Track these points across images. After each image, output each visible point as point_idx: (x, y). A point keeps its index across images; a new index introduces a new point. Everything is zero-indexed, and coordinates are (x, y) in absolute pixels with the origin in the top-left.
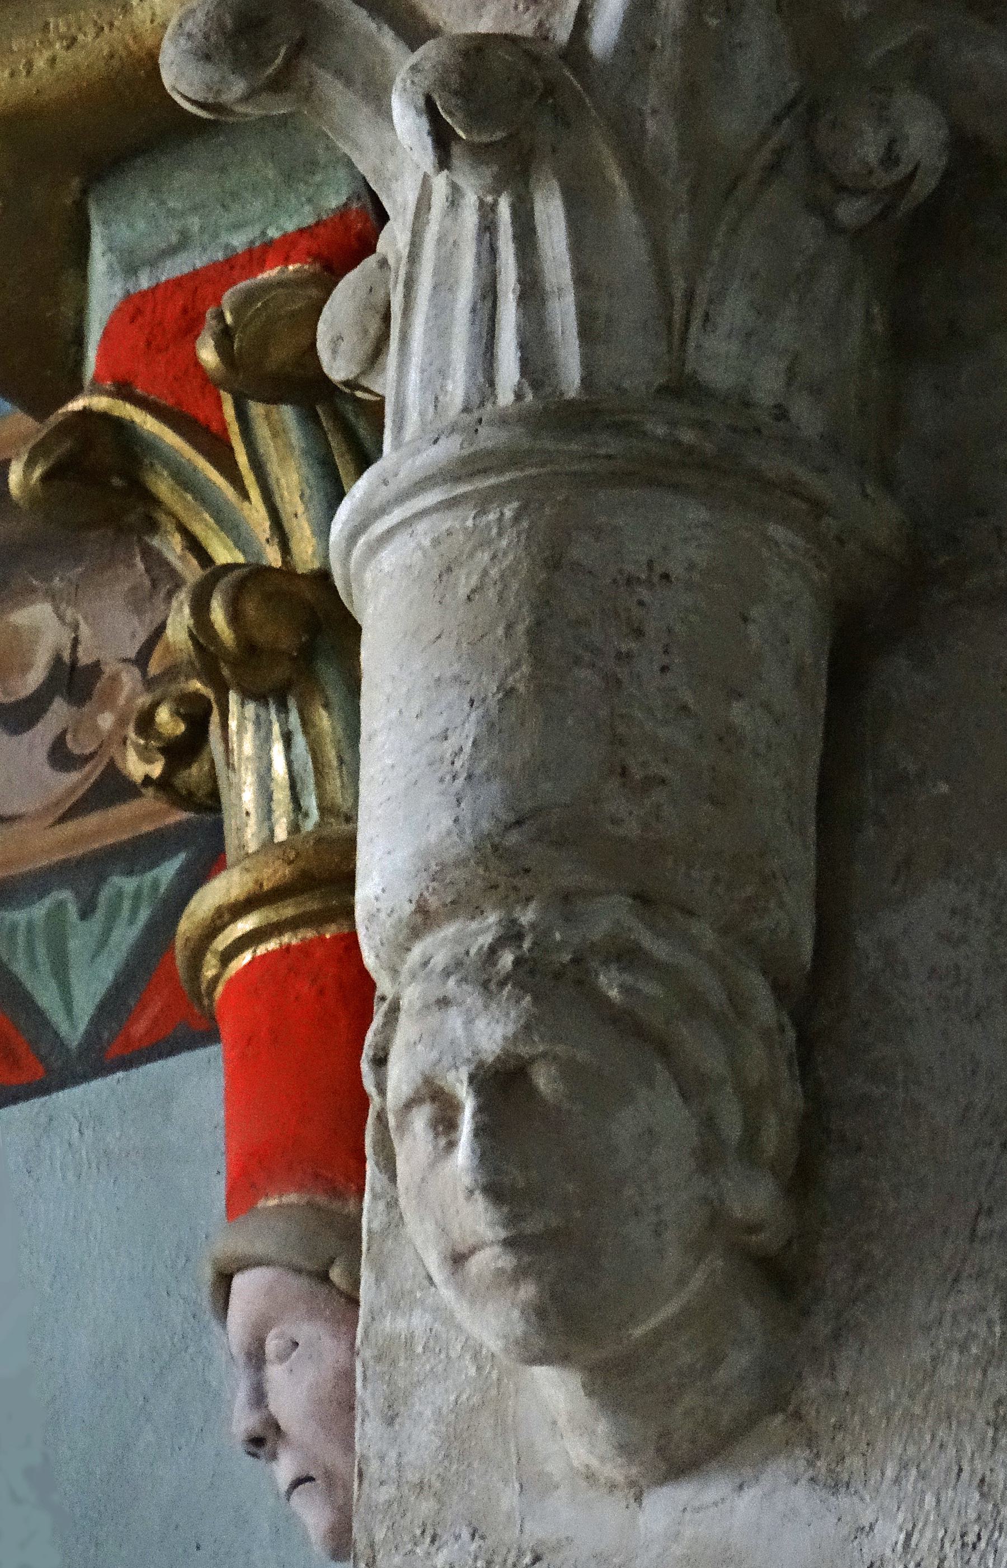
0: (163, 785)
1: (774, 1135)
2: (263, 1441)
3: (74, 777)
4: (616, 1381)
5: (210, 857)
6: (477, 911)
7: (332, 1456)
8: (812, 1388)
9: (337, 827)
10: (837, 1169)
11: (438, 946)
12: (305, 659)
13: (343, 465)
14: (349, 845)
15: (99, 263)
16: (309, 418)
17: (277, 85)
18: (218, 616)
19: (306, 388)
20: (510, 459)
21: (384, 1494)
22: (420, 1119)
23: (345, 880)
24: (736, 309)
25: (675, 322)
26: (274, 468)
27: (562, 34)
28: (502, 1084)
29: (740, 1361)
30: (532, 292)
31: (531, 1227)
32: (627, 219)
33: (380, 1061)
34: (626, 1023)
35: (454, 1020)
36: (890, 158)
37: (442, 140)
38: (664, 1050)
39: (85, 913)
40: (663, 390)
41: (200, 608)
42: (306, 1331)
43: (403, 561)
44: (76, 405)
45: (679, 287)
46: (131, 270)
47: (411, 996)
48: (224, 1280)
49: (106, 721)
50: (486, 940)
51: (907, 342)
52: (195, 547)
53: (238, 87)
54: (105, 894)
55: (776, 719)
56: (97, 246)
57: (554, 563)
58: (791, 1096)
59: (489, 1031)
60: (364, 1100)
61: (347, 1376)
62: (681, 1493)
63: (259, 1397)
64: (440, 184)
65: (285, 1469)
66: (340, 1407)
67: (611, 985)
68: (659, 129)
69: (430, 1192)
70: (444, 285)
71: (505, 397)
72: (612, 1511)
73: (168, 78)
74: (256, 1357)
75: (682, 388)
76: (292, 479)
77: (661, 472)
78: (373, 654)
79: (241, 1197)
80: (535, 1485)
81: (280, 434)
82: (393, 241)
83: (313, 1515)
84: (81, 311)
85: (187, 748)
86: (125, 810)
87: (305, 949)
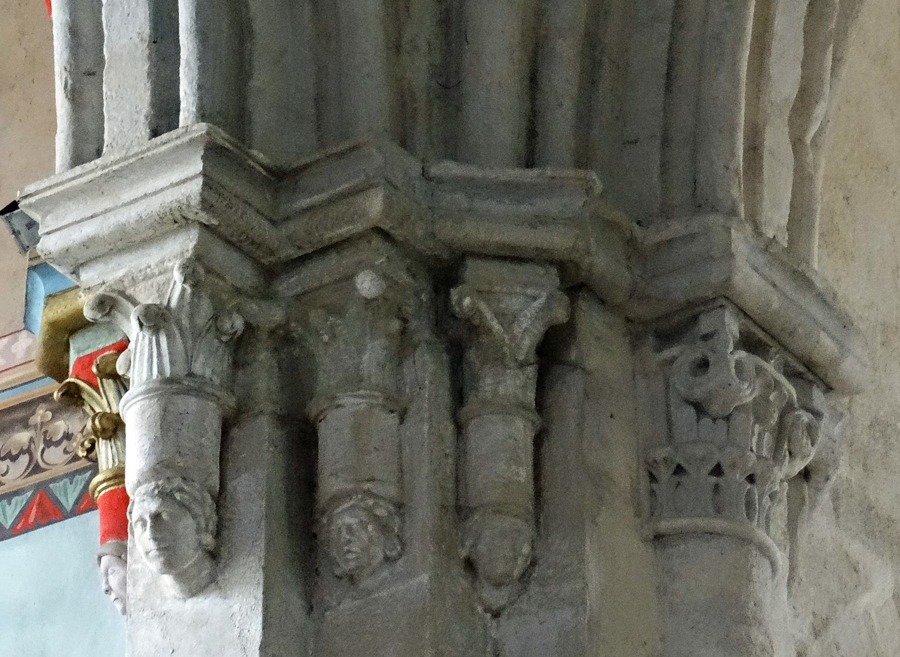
0: (86, 457)
1: (212, 527)
2: (108, 591)
3: (68, 456)
4: (181, 577)
5: (96, 472)
6: (150, 482)
7: (122, 593)
8: (220, 578)
9: (122, 466)
10: (225, 533)
11: (142, 489)
12: (115, 431)
13: (122, 390)
14: (123, 469)
15: (72, 352)
16: (115, 381)
17: (108, 314)
18: (97, 422)
19: (115, 377)
20: (156, 390)
21: (133, 602)
22: (139, 524)
23: (123, 476)
24: (201, 359)
25: (189, 360)
26: (108, 393)
27: (165, 303)
28: (156, 517)
29: (205, 573)
30: (160, 355)
31: (162, 546)
32: (179, 341)
33: (131, 513)
34: (182, 505)
35: (146, 504)
36: (232, 327)
37: (141, 325)
38: (189, 510)
39: (71, 483)
40: (187, 375)
41: (93, 420)
42: (117, 568)
43: (136, 411)
44: (67, 380)
45: (190, 354)
46: (78, 352)
47: (137, 500)
48: (100, 558)
49: (75, 444)
50: (152, 488)
51: (237, 365)
52: (92, 409)
53: (100, 315)
54: (75, 479)
55: (211, 442)
56: (71, 348)
57: (165, 411)
58: (215, 518)
59: (153, 506)
60: (127, 521)
61: (125, 577)
62: (195, 599)
63: (107, 582)
64: (141, 334)
65: (113, 596)
66: (123, 584)
67: (178, 496)
68: (185, 322)
69: (141, 539)
70: (142, 354)
71: (155, 377)
72: (179, 604)
73: (85, 314)
74: (107, 574)
75: (191, 375)
76: (112, 394)
77: (187, 391)
78: (129, 430)
79: (104, 539)
80: (164, 599)
81: (109, 384)
82: (131, 346)
83: (118, 606)
84: (68, 361)
85: (91, 450)
86: (78, 463)
87: (115, 491)
